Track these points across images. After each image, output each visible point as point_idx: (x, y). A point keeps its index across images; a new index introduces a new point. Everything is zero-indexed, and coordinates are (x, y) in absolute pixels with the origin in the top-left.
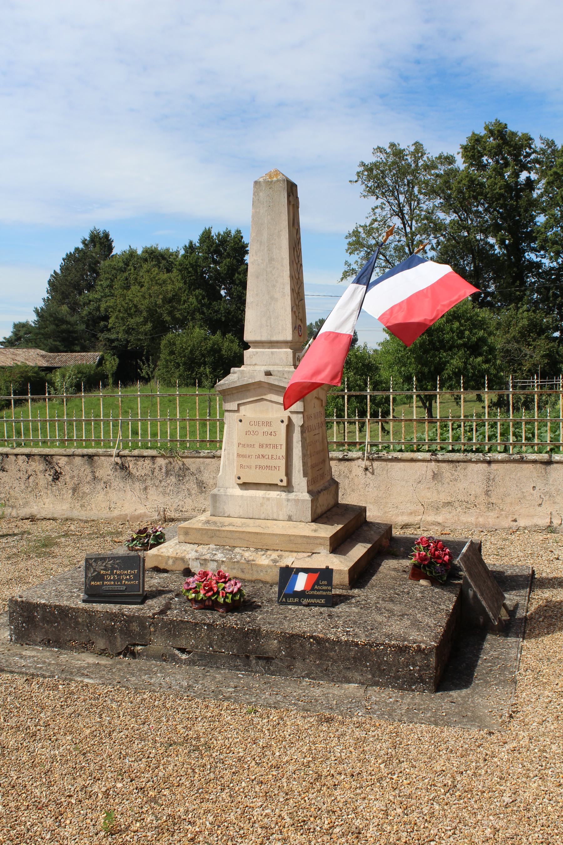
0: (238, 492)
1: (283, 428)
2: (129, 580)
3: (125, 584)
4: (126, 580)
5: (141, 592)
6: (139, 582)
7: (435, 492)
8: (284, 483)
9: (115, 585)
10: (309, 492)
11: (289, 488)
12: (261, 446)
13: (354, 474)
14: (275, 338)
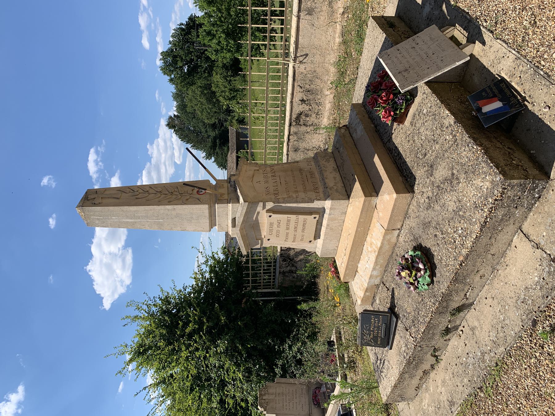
0: (320, 242)
1: (276, 217)
2: (379, 321)
4: (378, 323)
6: (381, 315)
7: (321, 13)
8: (317, 216)
10: (325, 200)
11: (321, 212)
12: (288, 229)
13: (304, 70)
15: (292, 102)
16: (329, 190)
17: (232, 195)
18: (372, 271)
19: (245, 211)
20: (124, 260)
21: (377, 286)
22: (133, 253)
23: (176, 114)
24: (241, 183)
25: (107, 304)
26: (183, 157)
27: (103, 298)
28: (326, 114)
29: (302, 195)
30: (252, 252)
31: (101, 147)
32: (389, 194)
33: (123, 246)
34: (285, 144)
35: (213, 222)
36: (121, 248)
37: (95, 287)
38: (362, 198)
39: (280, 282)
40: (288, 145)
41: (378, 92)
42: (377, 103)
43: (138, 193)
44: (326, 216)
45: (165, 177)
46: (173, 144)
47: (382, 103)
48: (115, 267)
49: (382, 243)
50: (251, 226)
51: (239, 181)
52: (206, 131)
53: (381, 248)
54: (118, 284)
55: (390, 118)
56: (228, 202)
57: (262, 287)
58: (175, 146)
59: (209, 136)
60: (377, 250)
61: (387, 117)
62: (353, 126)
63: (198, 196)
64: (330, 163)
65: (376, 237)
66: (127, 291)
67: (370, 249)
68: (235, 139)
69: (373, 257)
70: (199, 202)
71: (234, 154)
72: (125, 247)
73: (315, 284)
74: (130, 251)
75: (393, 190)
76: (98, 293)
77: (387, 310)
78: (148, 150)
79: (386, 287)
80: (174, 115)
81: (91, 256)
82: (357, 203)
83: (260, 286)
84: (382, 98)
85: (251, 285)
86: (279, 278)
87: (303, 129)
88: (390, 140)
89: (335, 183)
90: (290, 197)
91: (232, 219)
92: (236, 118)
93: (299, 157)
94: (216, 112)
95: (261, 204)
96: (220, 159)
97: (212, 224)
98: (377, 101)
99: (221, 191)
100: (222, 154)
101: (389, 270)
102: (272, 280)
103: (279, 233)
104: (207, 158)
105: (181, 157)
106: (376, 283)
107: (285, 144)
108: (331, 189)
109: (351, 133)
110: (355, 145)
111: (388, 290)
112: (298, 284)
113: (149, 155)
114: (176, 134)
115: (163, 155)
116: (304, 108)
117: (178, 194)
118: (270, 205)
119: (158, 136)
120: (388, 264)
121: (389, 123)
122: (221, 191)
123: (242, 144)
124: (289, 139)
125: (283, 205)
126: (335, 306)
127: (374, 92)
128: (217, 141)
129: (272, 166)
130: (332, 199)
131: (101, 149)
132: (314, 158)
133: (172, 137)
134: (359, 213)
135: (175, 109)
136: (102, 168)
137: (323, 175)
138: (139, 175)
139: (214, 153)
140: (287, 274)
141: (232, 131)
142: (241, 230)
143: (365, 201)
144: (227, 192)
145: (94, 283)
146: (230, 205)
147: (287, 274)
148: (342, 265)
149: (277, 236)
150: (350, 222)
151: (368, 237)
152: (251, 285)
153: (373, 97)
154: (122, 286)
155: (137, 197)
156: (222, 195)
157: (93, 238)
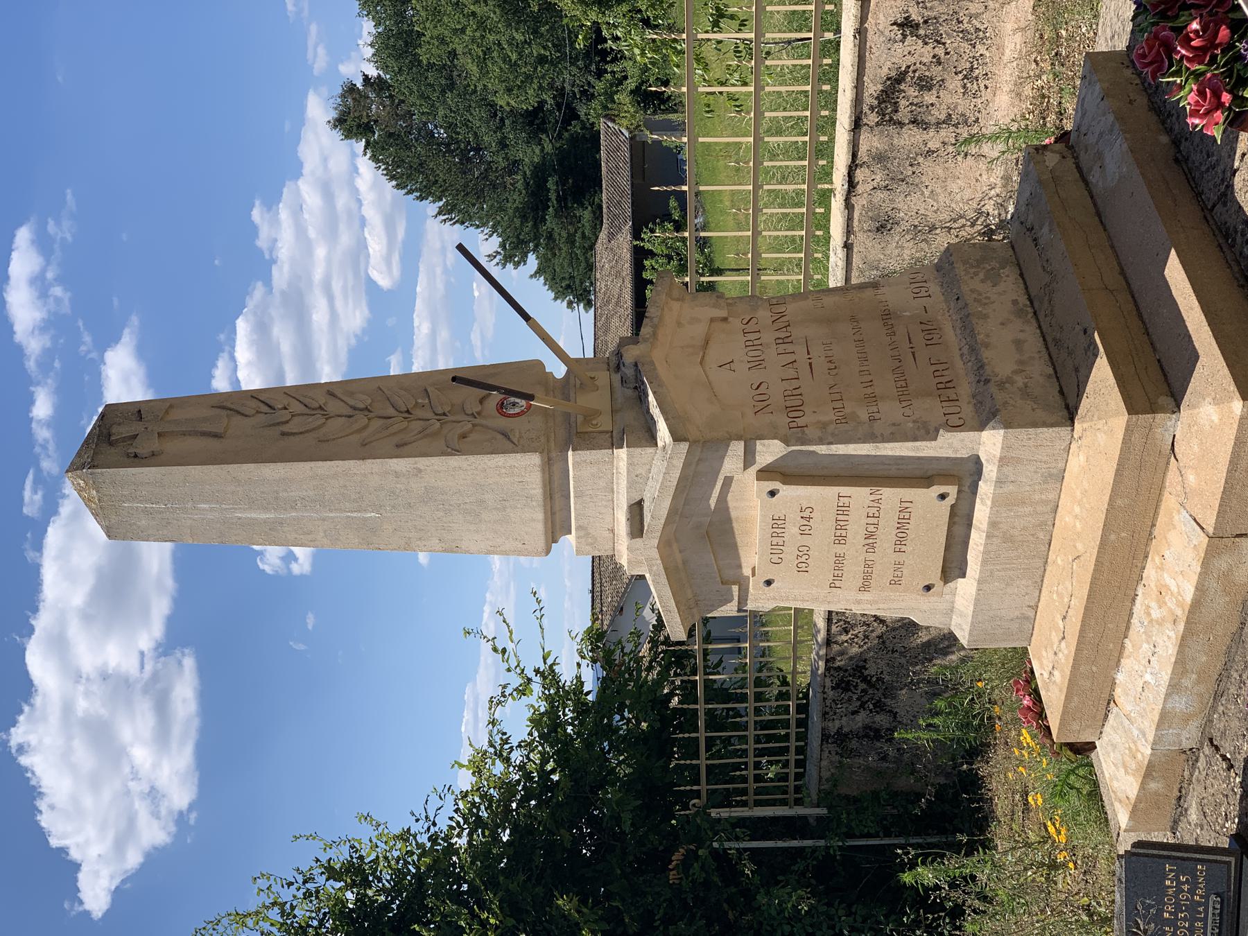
0: (965, 589)
3: (1207, 897)
4: (1192, 892)
5: (1232, 860)
8: (952, 490)
9: (1205, 920)
10: (981, 427)
11: (966, 474)
12: (840, 540)
14: (537, 491)
15: (861, 32)
16: (993, 388)
17: (629, 417)
18: (1168, 695)
19: (676, 474)
20: (162, 706)
21: (1191, 755)
22: (203, 671)
23: (373, 72)
24: (662, 370)
25: (95, 893)
26: (403, 259)
27: (76, 867)
28: (1006, 76)
29: (891, 410)
30: (706, 653)
31: (58, 223)
32: (1216, 402)
33: (158, 645)
34: (837, 204)
35: (558, 517)
36: (149, 656)
37: (45, 820)
38: (1120, 420)
39: (826, 774)
40: (848, 205)
41: (1177, 17)
42: (1170, 59)
43: (285, 415)
44: (985, 488)
45: (322, 349)
46: (359, 202)
47: (1189, 59)
48: (126, 733)
49: (1200, 589)
50: (699, 534)
51: (652, 363)
52: (503, 144)
53: (1196, 604)
54: (142, 809)
55: (1220, 116)
56: (615, 443)
57: (751, 797)
58: (369, 212)
59: (514, 166)
60: (1181, 614)
61: (1208, 113)
62: (1092, 139)
63: (502, 422)
64: (1001, 287)
65: (1175, 567)
66: (178, 837)
67: (1156, 614)
68: (626, 172)
69: (1168, 642)
70: (508, 443)
71: (624, 240)
72: (168, 647)
73: (973, 783)
74: (189, 663)
75: (1233, 388)
76: (54, 842)
77: (1225, 843)
78: (254, 230)
79: (1224, 758)
80: (366, 79)
81: (25, 688)
82: (1101, 438)
83: (744, 792)
84: (1186, 42)
85: (703, 787)
86: (821, 762)
87: (910, 138)
88: (1224, 195)
89: (1021, 362)
90: (845, 420)
91: (631, 507)
92: (631, 84)
93: (898, 253)
94: (542, 60)
95: (737, 448)
96: (561, 262)
97: (556, 526)
98: (1170, 50)
99: (587, 400)
100: (571, 240)
101: (1233, 690)
102: (792, 783)
103: (814, 559)
104: (508, 258)
105: (396, 258)
106: (1186, 745)
107: (837, 204)
108: (1001, 385)
109: (1084, 165)
110: (1098, 214)
111: (1231, 767)
112: (905, 782)
113: (261, 251)
114: (374, 158)
115: (321, 252)
116: (917, 52)
117: (430, 415)
118: (770, 451)
119: (296, 171)
120: (1226, 668)
121: (1217, 133)
122: (587, 400)
123: (660, 194)
124: (852, 184)
125: (822, 449)
126: (1054, 866)
127: (1163, 16)
128: (551, 184)
129: (777, 303)
130: (1007, 425)
131: (62, 230)
132: (938, 268)
133: (355, 170)
134: (1110, 477)
135: (369, 52)
136: (66, 308)
137: (973, 334)
138: (222, 337)
139: (536, 238)
140: (854, 744)
141: (615, 136)
142: (665, 545)
143: (1129, 430)
144: (607, 404)
145: (42, 805)
146: (622, 454)
147: (854, 744)
148: (1052, 670)
149: (802, 568)
150: (1077, 509)
151: (1149, 565)
152: (703, 787)
153: (1156, 36)
154: (156, 815)
155: (285, 428)
156: (590, 416)
157: (35, 610)
